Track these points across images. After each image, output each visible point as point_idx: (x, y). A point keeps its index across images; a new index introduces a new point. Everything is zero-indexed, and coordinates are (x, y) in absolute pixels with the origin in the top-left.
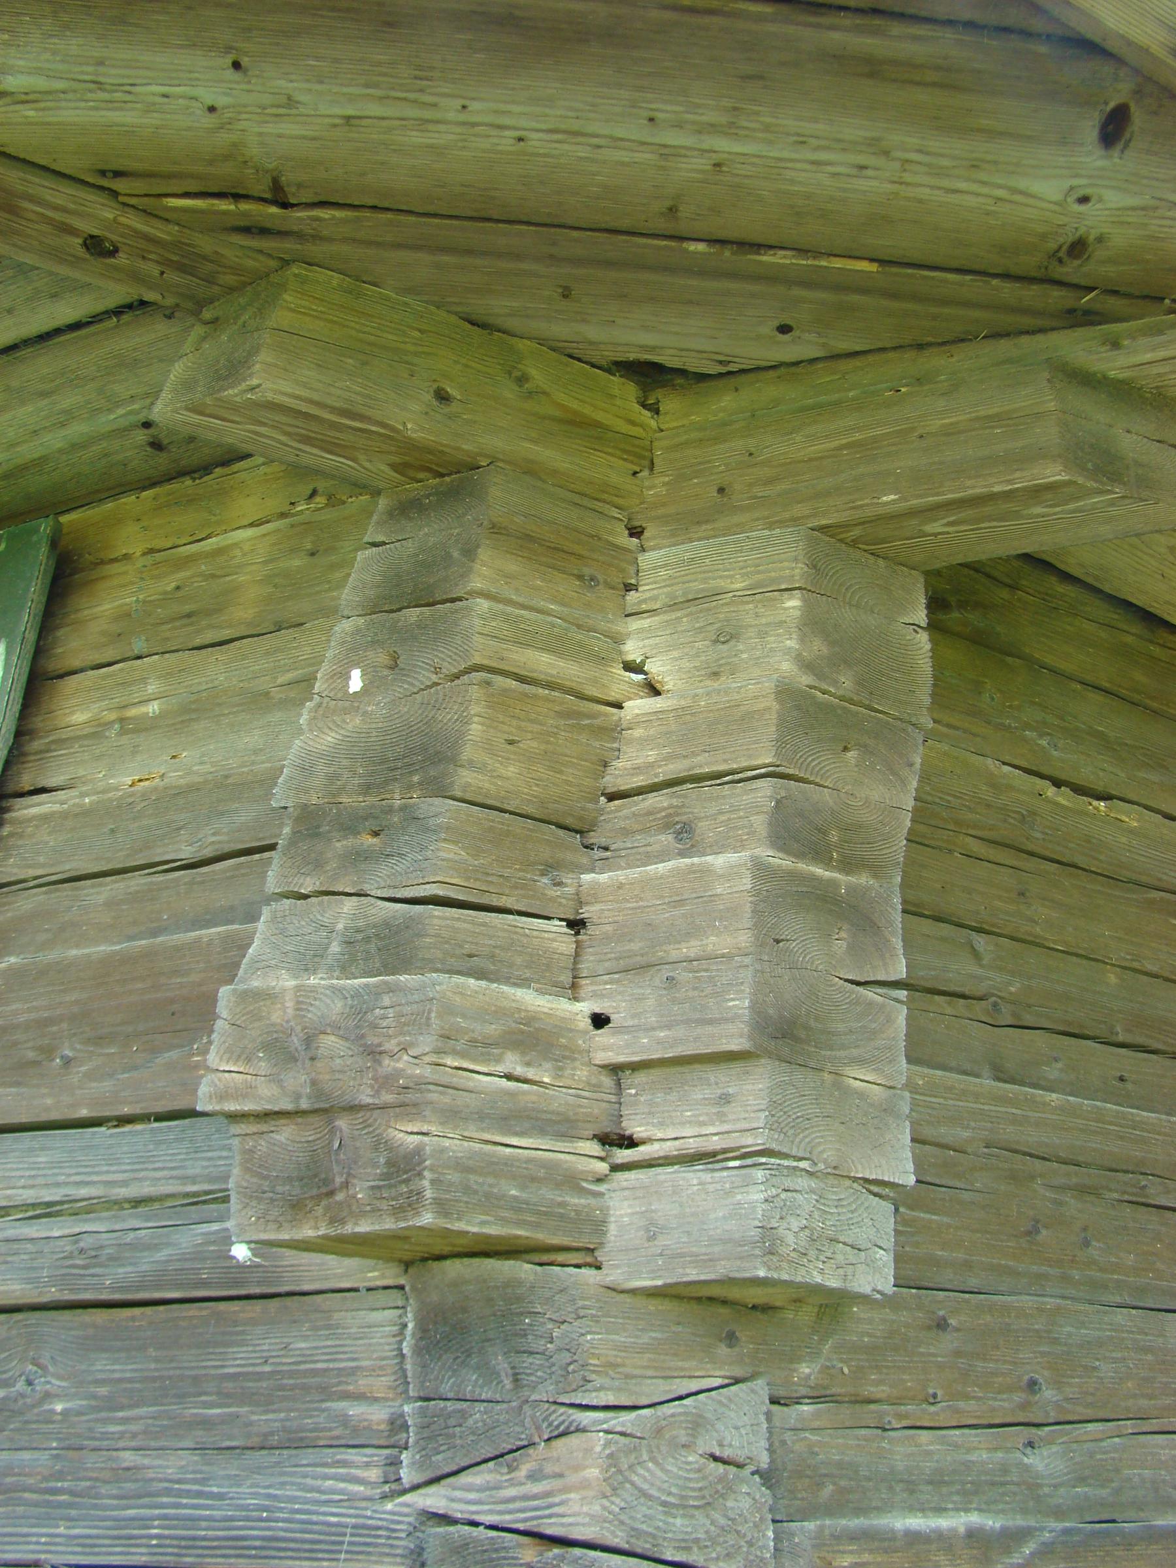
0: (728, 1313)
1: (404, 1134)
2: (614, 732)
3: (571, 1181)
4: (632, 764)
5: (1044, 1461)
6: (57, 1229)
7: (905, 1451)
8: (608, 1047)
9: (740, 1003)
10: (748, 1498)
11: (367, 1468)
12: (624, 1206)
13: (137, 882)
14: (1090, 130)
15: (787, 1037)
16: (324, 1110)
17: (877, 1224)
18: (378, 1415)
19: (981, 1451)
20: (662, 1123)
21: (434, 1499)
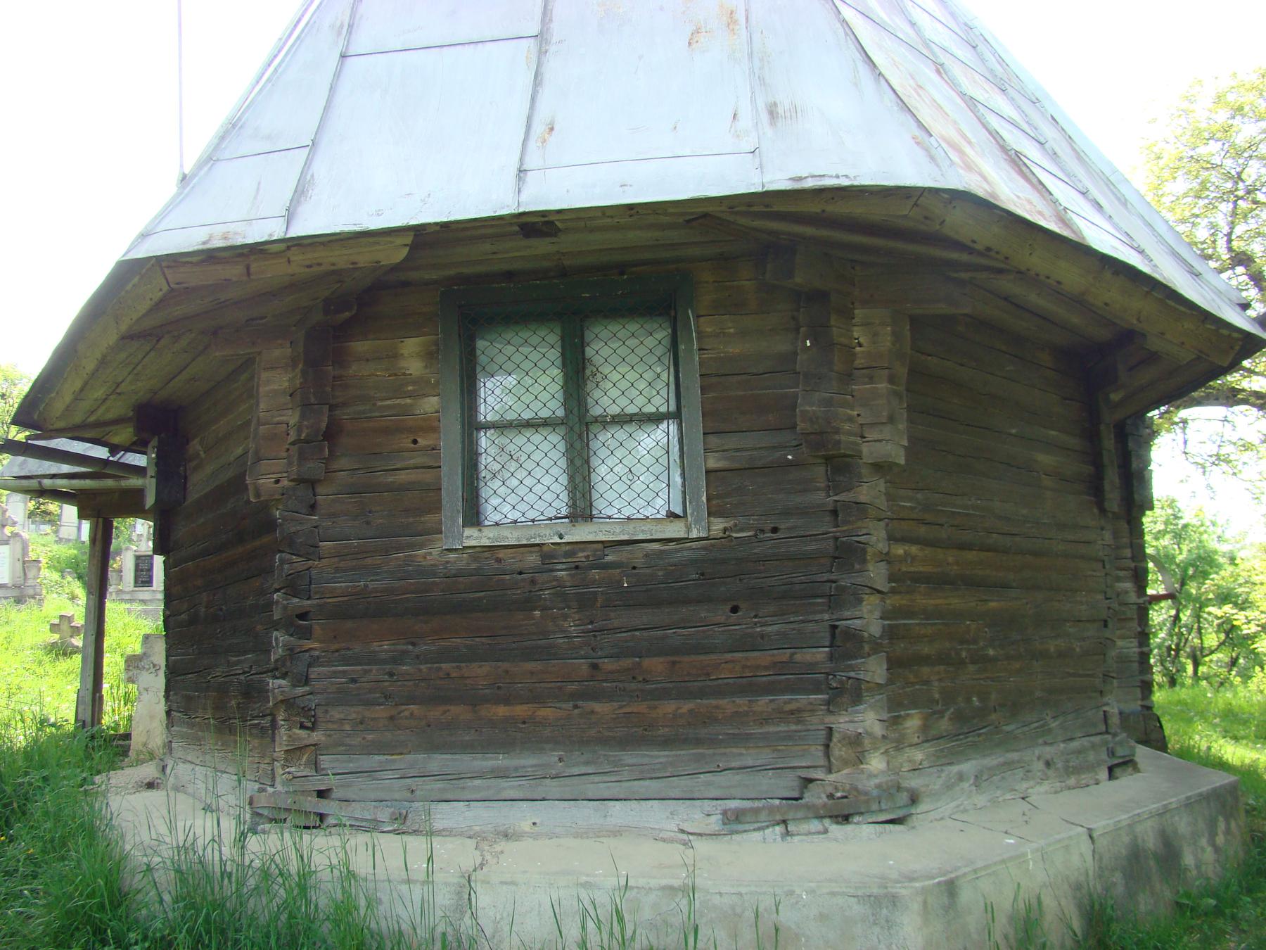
0: (880, 468)
1: (837, 437)
2: (854, 355)
3: (857, 444)
4: (859, 362)
5: (919, 496)
6: (744, 454)
7: (902, 492)
8: (860, 420)
9: (885, 414)
10: (883, 497)
11: (822, 494)
12: (865, 449)
13: (744, 377)
14: (1104, 774)
15: (891, 420)
16: (821, 433)
17: (902, 452)
18: (822, 485)
19: (910, 493)
20: (871, 435)
21: (836, 498)
